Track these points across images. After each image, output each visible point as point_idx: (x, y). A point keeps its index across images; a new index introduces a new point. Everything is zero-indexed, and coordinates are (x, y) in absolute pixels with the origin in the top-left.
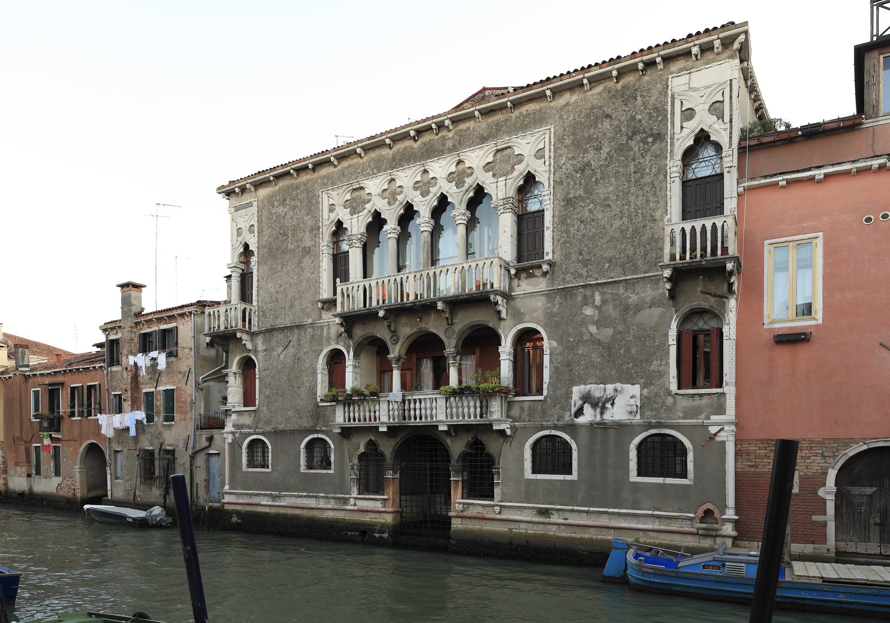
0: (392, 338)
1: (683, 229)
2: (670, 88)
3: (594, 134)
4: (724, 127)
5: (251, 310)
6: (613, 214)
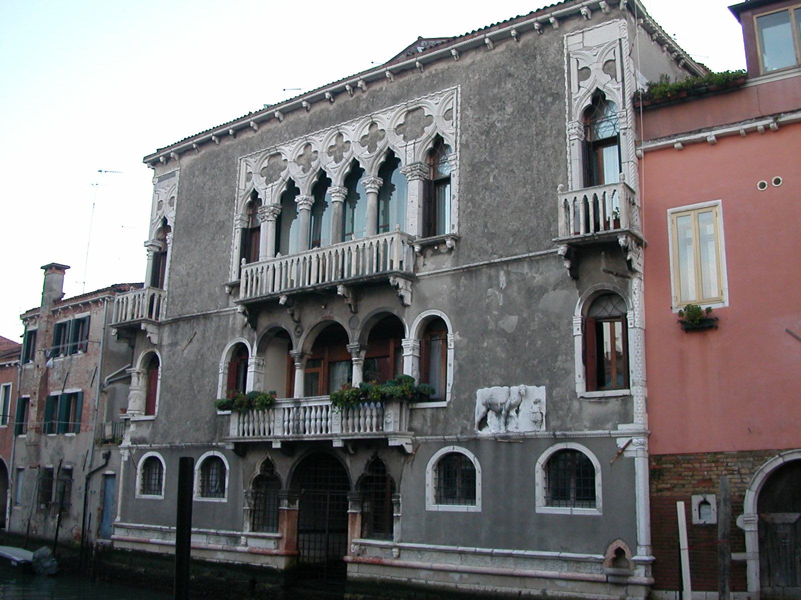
0: (296, 329)
1: (585, 196)
2: (565, 47)
3: (498, 93)
5: (160, 296)
6: (517, 180)
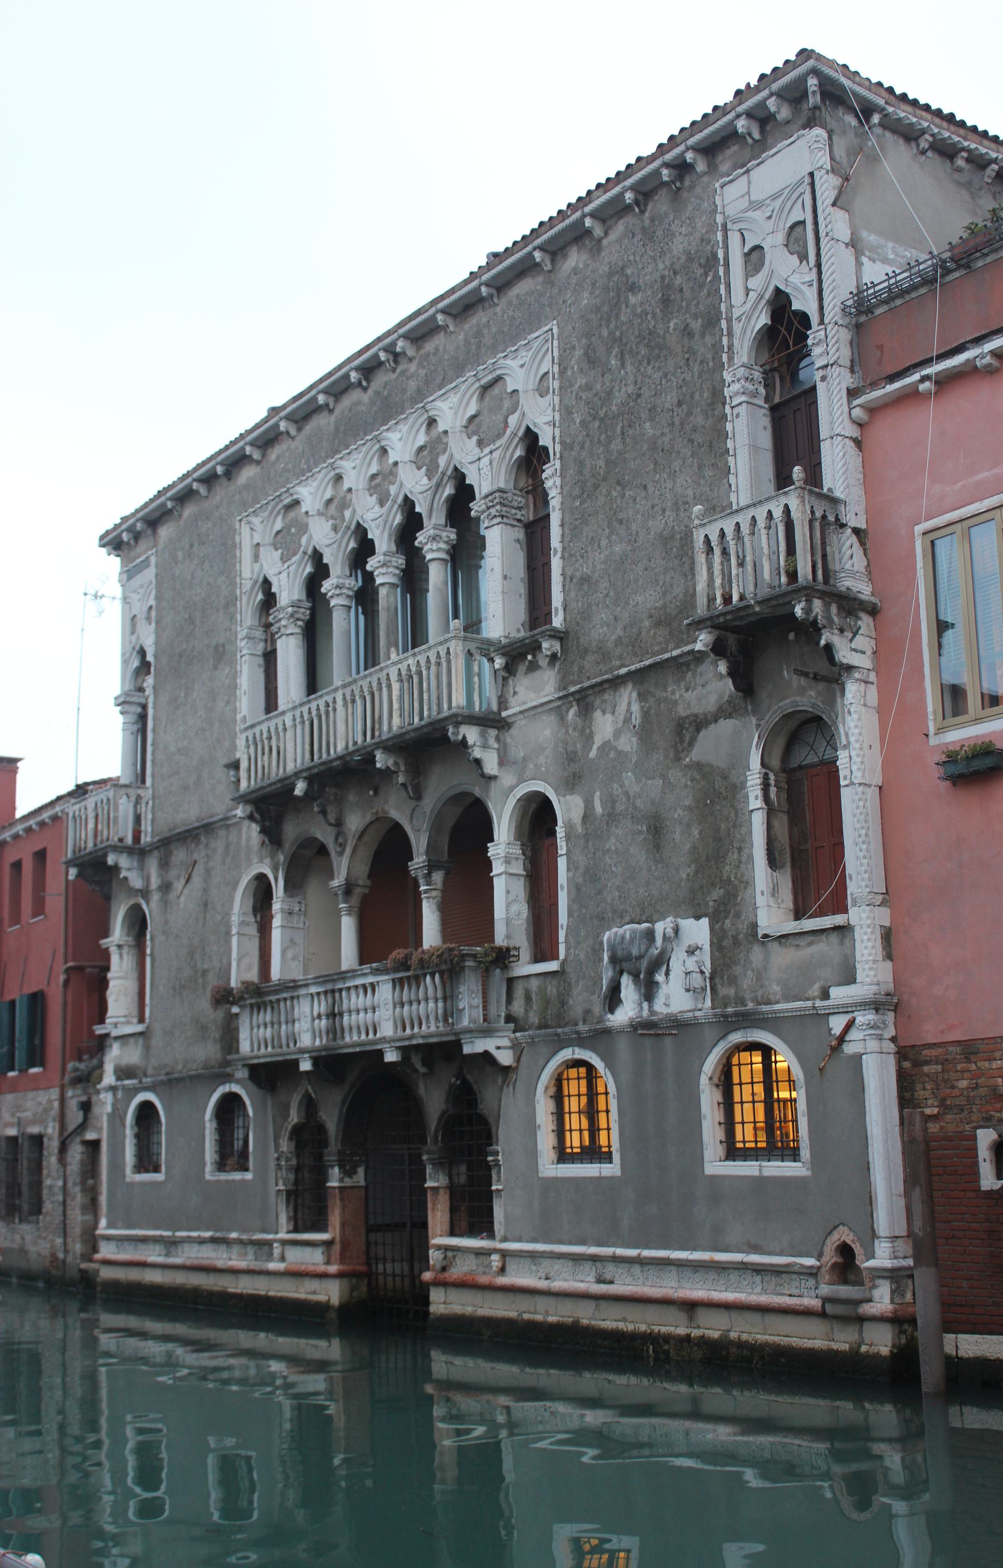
0: (336, 839)
4: (807, 279)
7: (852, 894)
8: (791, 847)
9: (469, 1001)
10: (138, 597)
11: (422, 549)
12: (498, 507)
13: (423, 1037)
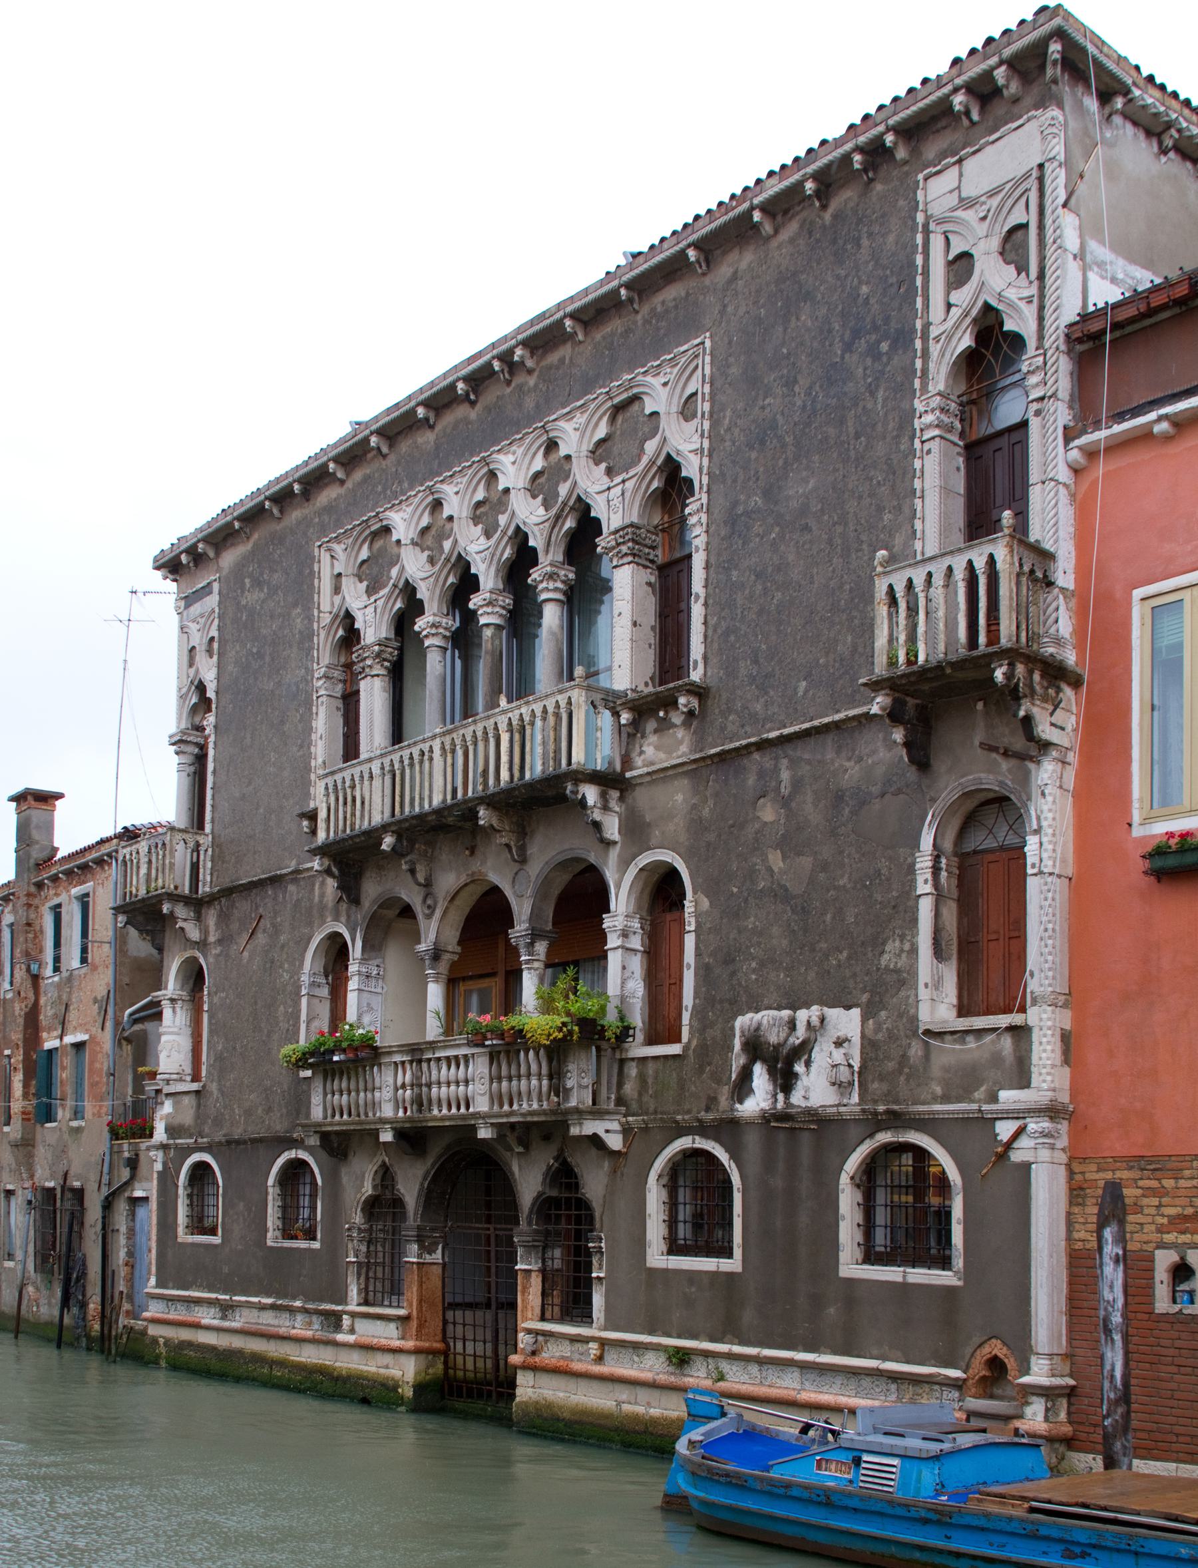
0: (424, 901)
4: (1026, 293)
7: (1032, 993)
8: (959, 937)
9: (580, 1079)
10: (198, 627)
11: (536, 587)
12: (630, 544)
13: (523, 1115)
